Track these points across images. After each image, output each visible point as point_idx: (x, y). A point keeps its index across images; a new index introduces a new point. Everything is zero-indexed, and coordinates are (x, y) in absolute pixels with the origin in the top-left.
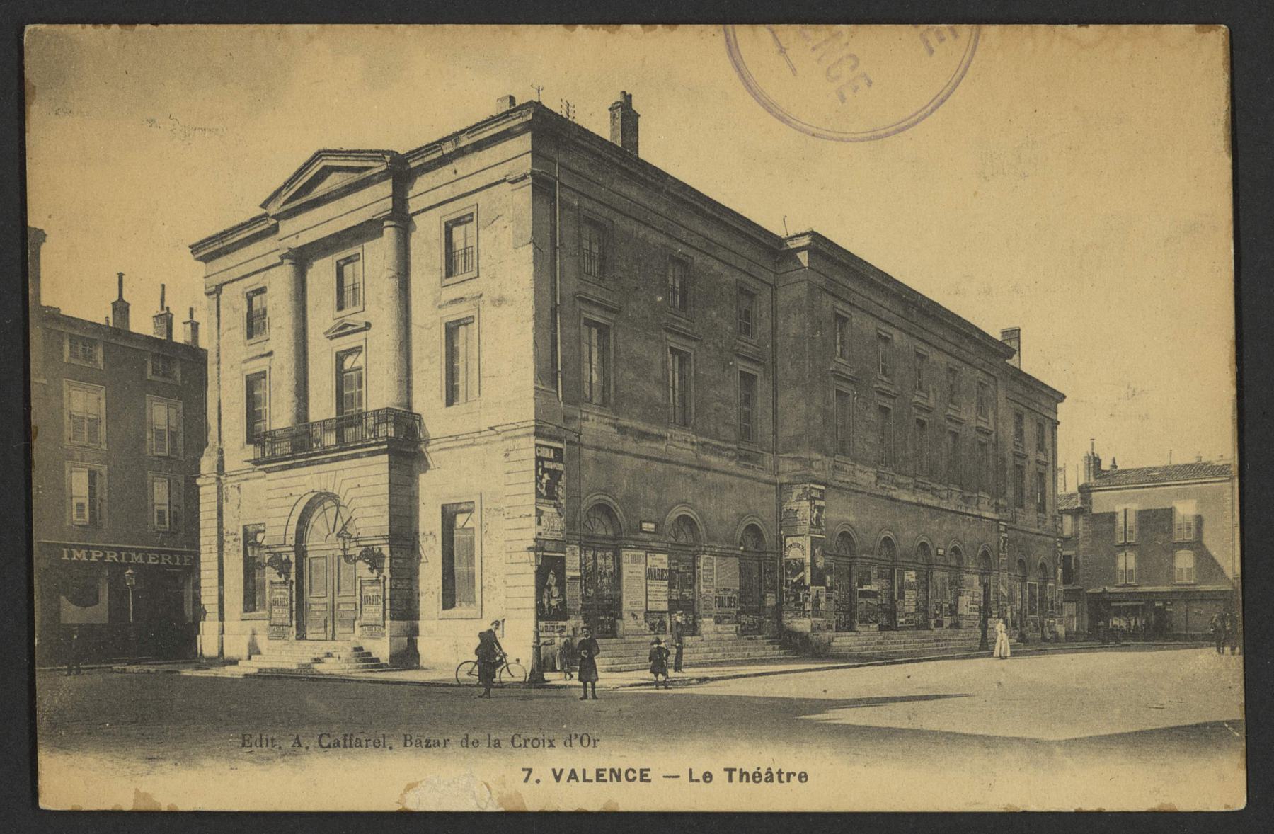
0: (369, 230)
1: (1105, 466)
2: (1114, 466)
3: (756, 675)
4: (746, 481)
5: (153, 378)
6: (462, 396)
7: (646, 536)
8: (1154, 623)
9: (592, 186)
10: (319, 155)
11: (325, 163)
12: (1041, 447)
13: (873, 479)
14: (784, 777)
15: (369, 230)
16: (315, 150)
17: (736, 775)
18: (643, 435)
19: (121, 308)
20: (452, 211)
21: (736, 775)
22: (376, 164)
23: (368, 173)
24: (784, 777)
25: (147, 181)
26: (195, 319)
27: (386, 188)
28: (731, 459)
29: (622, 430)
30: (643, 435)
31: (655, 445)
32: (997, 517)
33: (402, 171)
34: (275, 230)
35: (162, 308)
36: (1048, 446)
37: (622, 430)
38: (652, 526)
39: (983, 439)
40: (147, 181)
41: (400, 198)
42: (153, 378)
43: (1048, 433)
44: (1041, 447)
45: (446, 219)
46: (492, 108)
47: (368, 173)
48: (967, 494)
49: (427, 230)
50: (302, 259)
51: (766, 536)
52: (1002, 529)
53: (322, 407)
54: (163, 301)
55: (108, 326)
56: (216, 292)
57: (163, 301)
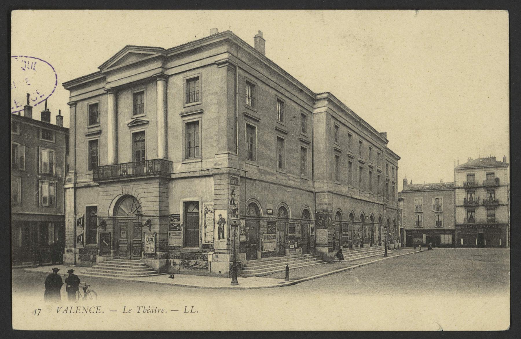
0: (152, 80)
1: (409, 183)
2: (411, 183)
3: (332, 274)
4: (303, 192)
8: (14, 213)
9: (250, 68)
10: (127, 47)
11: (130, 51)
13: (347, 190)
14: (157, 311)
15: (152, 80)
16: (125, 45)
17: (142, 310)
20: (191, 75)
21: (142, 310)
22: (155, 53)
23: (151, 57)
24: (157, 311)
26: (62, 115)
33: (166, 56)
34: (104, 79)
35: (46, 109)
38: (271, 211)
40: (53, 54)
43: (395, 171)
47: (151, 57)
49: (178, 83)
50: (117, 91)
55: (29, 119)
56: (73, 104)
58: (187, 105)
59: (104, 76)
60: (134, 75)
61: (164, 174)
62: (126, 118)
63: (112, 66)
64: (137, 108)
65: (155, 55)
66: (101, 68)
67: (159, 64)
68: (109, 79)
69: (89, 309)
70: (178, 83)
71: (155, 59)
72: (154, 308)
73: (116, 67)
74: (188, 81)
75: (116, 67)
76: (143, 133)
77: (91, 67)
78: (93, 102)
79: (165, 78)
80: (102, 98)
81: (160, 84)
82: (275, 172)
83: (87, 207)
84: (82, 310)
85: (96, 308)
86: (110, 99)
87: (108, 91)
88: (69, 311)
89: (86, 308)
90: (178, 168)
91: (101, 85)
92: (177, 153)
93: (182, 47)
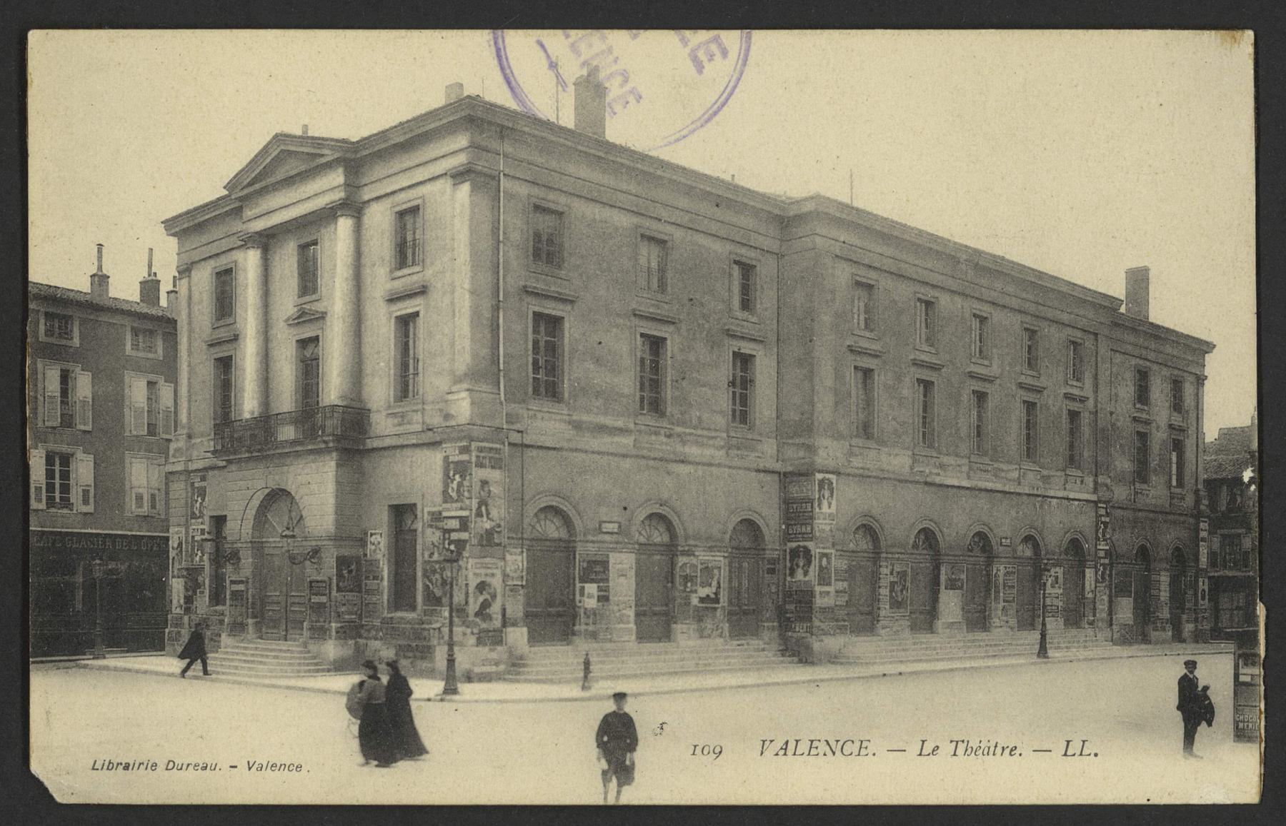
0: (328, 215)
5: (134, 353)
6: (411, 394)
7: (607, 538)
12: (1177, 406)
13: (908, 461)
14: (999, 750)
15: (328, 215)
17: (961, 747)
18: (602, 429)
19: (100, 279)
21: (961, 747)
23: (323, 160)
24: (999, 750)
25: (135, 145)
27: (337, 177)
28: (720, 448)
29: (578, 426)
30: (602, 429)
31: (616, 439)
32: (1094, 498)
33: (356, 159)
34: (238, 211)
36: (1189, 401)
37: (578, 426)
39: (1075, 406)
41: (352, 186)
42: (134, 353)
43: (1189, 390)
44: (1177, 406)
45: (398, 209)
46: (436, 100)
48: (1045, 472)
49: (379, 218)
50: (266, 241)
51: (764, 529)
52: (1102, 512)
53: (286, 398)
54: (150, 266)
57: (150, 266)
58: (399, 273)
59: (237, 204)
60: (269, 205)
61: (350, 437)
62: (287, 302)
63: (250, 184)
64: (308, 280)
65: (330, 155)
66: (231, 186)
67: (337, 177)
68: (248, 213)
69: (840, 744)
70: (379, 218)
71: (329, 166)
72: (992, 744)
73: (257, 186)
74: (401, 214)
75: (257, 186)
76: (317, 339)
77: (211, 189)
78: (223, 262)
79: (352, 206)
80: (238, 255)
81: (344, 225)
82: (632, 426)
83: (415, 505)
84: (823, 747)
85: (857, 744)
86: (250, 260)
87: (250, 241)
88: (790, 752)
89: (833, 744)
90: (383, 425)
91: (237, 226)
92: (379, 391)
93: (383, 135)
